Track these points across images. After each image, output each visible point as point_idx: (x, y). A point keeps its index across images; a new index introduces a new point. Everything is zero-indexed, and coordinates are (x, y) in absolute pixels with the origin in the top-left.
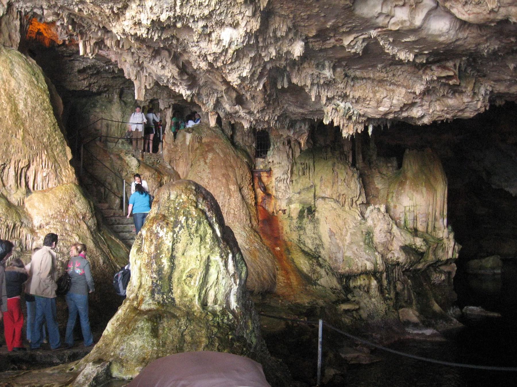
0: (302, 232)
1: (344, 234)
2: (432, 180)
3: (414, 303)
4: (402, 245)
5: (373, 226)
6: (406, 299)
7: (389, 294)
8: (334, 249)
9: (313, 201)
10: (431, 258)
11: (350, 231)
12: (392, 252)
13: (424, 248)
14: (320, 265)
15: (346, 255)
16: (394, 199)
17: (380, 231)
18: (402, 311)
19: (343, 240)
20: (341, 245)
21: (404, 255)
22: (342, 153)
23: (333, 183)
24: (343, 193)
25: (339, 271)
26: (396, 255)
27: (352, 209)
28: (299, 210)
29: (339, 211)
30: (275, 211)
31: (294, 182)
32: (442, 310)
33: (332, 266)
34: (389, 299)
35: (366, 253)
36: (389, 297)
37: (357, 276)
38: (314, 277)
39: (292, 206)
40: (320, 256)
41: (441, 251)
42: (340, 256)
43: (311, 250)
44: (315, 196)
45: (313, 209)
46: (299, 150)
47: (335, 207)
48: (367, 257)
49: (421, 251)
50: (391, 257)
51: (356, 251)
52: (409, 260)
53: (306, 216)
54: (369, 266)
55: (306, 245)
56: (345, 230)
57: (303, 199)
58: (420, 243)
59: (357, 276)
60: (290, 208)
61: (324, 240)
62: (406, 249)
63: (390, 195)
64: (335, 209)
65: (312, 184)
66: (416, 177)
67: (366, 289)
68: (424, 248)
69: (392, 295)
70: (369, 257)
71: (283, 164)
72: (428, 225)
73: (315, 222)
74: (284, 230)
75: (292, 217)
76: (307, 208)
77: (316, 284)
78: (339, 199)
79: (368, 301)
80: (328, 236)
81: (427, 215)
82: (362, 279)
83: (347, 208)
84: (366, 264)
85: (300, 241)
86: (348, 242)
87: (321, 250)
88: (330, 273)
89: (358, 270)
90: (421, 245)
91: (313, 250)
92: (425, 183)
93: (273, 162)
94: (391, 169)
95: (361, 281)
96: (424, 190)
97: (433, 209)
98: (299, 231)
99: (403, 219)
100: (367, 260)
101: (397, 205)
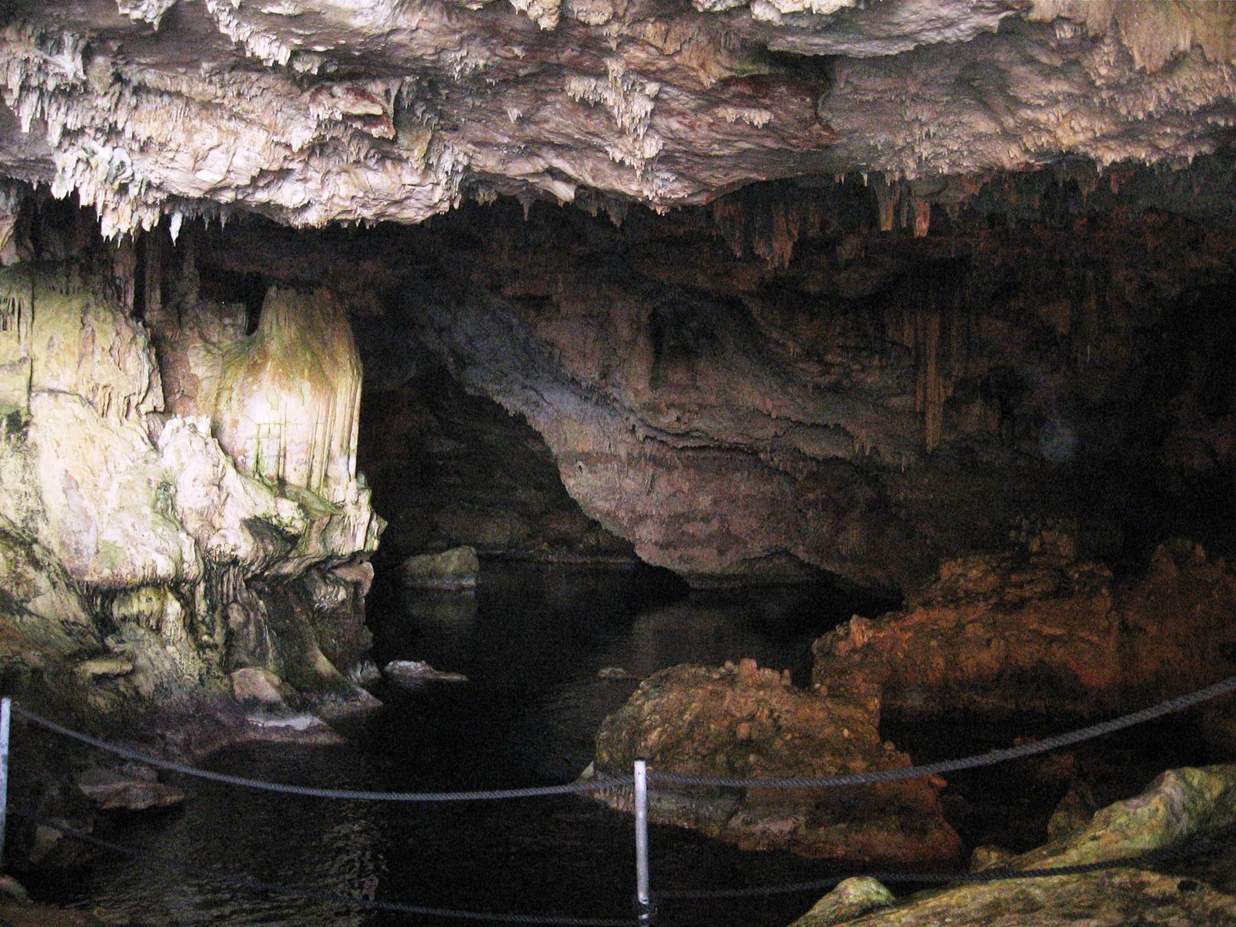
1: (101, 485)
4: (248, 517)
5: (176, 468)
7: (211, 635)
10: (314, 549)
11: (118, 479)
14: (36, 564)
16: (234, 403)
17: (195, 480)
18: (241, 676)
20: (92, 512)
22: (110, 281)
23: (82, 356)
24: (104, 382)
25: (87, 578)
32: (335, 671)
36: (211, 641)
37: (132, 590)
38: (18, 593)
40: (35, 541)
41: (339, 532)
42: (88, 540)
43: (12, 524)
44: (30, 387)
45: (24, 419)
47: (81, 417)
49: (293, 531)
50: (219, 546)
51: (131, 529)
52: (261, 554)
54: (165, 568)
56: (104, 475)
59: (132, 590)
62: (258, 527)
63: (225, 395)
64: (82, 422)
66: (289, 353)
67: (153, 622)
69: (219, 638)
70: (165, 545)
72: (311, 471)
77: (22, 611)
78: (94, 397)
81: (312, 447)
84: (154, 562)
86: (111, 505)
87: (41, 525)
88: (62, 584)
89: (135, 576)
90: (293, 518)
91: (19, 524)
94: (231, 331)
95: (141, 604)
96: (307, 386)
97: (325, 434)
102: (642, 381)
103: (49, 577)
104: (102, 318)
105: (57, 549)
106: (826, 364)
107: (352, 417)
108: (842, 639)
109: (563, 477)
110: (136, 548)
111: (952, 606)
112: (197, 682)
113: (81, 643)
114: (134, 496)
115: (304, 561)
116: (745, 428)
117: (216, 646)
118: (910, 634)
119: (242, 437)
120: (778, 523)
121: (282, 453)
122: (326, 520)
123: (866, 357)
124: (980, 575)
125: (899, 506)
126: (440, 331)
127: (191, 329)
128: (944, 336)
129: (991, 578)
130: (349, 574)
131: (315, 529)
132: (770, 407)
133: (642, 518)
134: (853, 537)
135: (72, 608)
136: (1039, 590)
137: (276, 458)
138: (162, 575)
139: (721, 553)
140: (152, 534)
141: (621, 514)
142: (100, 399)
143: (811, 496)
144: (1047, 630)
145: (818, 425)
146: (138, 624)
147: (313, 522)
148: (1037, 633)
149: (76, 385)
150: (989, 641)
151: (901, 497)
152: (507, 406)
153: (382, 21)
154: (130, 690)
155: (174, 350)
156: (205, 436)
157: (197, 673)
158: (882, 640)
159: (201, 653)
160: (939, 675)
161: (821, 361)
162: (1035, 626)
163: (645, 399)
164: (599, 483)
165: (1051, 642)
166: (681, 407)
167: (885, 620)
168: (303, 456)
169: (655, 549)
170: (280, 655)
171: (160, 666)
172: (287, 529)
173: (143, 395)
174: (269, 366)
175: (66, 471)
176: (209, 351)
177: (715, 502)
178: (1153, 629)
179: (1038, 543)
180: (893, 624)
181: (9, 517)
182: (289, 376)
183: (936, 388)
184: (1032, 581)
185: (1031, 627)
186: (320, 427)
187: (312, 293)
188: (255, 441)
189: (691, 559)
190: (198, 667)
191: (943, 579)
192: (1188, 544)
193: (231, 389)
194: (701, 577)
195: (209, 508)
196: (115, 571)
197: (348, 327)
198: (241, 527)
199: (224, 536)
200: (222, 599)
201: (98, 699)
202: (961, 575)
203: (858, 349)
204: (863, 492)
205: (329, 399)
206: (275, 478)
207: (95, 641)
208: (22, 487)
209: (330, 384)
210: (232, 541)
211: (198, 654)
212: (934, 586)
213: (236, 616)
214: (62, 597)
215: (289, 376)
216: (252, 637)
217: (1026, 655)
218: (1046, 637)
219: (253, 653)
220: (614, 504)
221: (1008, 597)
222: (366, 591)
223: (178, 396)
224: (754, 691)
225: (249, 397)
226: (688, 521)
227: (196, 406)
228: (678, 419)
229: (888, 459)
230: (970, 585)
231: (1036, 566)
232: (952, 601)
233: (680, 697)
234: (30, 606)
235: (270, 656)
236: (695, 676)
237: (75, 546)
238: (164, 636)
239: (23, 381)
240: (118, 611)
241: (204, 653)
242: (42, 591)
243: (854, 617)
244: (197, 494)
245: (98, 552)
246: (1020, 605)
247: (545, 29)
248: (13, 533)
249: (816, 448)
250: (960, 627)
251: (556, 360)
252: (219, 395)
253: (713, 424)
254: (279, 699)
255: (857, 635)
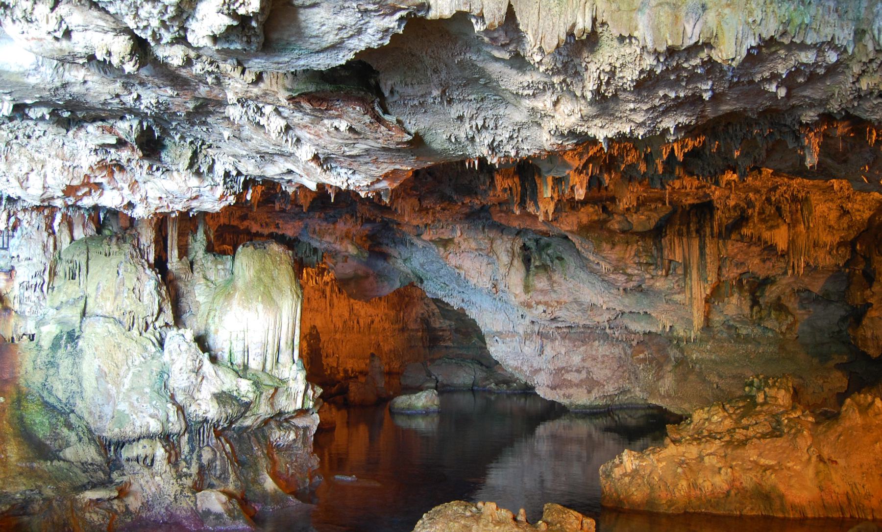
0: (52, 371)
1: (122, 374)
2: (274, 293)
3: (231, 480)
4: (216, 391)
5: (170, 362)
6: (218, 473)
7: (189, 468)
8: (99, 399)
9: (79, 321)
10: (264, 410)
11: (133, 370)
12: (198, 402)
13: (251, 396)
14: (70, 426)
15: (119, 408)
16: (216, 319)
17: (181, 369)
18: (201, 496)
19: (118, 385)
20: (113, 391)
21: (217, 406)
22: (137, 247)
23: (117, 294)
24: (129, 309)
25: (104, 434)
26: (204, 407)
27: (144, 334)
28: (55, 335)
29: (121, 339)
30: (15, 336)
31: (55, 289)
32: (276, 487)
33: (93, 427)
34: (186, 475)
35: (152, 405)
36: (189, 472)
37: (134, 441)
38: (54, 446)
39: (45, 329)
40: (73, 411)
41: (284, 398)
42: (108, 410)
43: (60, 401)
44: (84, 314)
45: (77, 334)
46: (68, 240)
47: (113, 332)
48: (152, 411)
49: (246, 400)
50: (195, 411)
51: (136, 403)
52: (224, 415)
53: (63, 346)
54: (155, 427)
55: (54, 392)
56: (125, 367)
57: (63, 317)
58: (247, 388)
59: (134, 441)
60: (41, 333)
61: (86, 384)
62: (222, 398)
63: (212, 314)
64: (113, 335)
65: (82, 294)
66: (250, 287)
67: (148, 461)
68: (251, 396)
69: (194, 469)
70: (156, 412)
71: (35, 260)
72: (265, 360)
73: (77, 355)
74: (23, 368)
75: (41, 347)
76: (68, 333)
78: (124, 319)
79: (147, 482)
80: (94, 377)
81: (265, 345)
82: (140, 447)
83: (135, 332)
84: (148, 423)
85: (45, 385)
86: (126, 387)
87: (78, 402)
88: (85, 439)
89: (134, 432)
90: (248, 391)
91: (64, 401)
92: (262, 297)
93: (18, 256)
94: (222, 273)
95: (137, 450)
96: (260, 307)
97: (274, 336)
98: (48, 369)
99: (227, 351)
100: (151, 416)
101: (220, 329)
102: (518, 288)
103: (77, 435)
104: (129, 270)
105: (86, 416)
106: (629, 275)
107: (294, 325)
108: (617, 466)
109: (488, 346)
110: (136, 414)
111: (695, 443)
112: (172, 500)
113: (92, 477)
114: (141, 381)
115: (258, 418)
116: (589, 315)
117: (191, 475)
118: (664, 463)
119: (220, 341)
120: (623, 373)
121: (246, 349)
122: (272, 391)
123: (654, 270)
124: (720, 420)
125: (695, 362)
126: (405, 260)
127: (198, 272)
128: (702, 254)
129: (728, 422)
130: (300, 422)
131: (263, 396)
132: (601, 302)
133: (537, 371)
134: (668, 383)
135: (90, 454)
136: (760, 431)
137: (242, 353)
138: (153, 431)
139: (589, 392)
140: (148, 405)
141: (525, 368)
142: (127, 320)
143: (641, 356)
144: (763, 461)
145: (634, 313)
146: (138, 462)
147: (261, 393)
148: (756, 463)
149: (113, 312)
150: (720, 469)
151: (694, 356)
152: (452, 304)
153: (49, 79)
154: (121, 508)
155: (186, 286)
156: (189, 341)
157: (173, 493)
158: (644, 467)
159: (179, 480)
160: (683, 493)
161: (625, 273)
162: (755, 458)
163: (522, 299)
164: (509, 350)
165: (765, 471)
166: (546, 304)
167: (648, 453)
168: (259, 351)
169: (548, 390)
170: (238, 478)
171: (148, 490)
172: (242, 399)
173: (155, 316)
174: (237, 295)
175: (99, 366)
176: (208, 286)
177: (583, 360)
178: (842, 462)
179: (763, 396)
180: (651, 456)
181: (59, 396)
182: (248, 301)
183: (699, 290)
184: (757, 423)
185: (752, 459)
186: (271, 332)
187: (265, 248)
188: (228, 342)
189: (569, 396)
190: (175, 490)
191: (695, 422)
192: (870, 398)
193: (216, 310)
194: (577, 406)
195: (189, 387)
196: (122, 430)
197: (290, 268)
198: (211, 398)
199: (199, 404)
200: (199, 444)
201: (93, 515)
202: (707, 419)
203: (648, 264)
204: (673, 353)
205: (276, 313)
206: (242, 365)
207: (103, 476)
208: (70, 377)
209: (277, 305)
210: (204, 407)
211: (177, 481)
212: (688, 427)
213: (207, 455)
214: (85, 447)
215: (248, 301)
216: (218, 468)
217: (748, 480)
218: (762, 466)
219: (219, 478)
220: (520, 362)
221: (737, 436)
222: (313, 433)
223: (188, 314)
224: (492, 526)
225: (225, 315)
226: (567, 372)
227: (197, 321)
228: (544, 312)
229: (682, 334)
230: (713, 427)
231: (760, 413)
232: (696, 439)
233: (443, 528)
234: (61, 454)
235: (231, 479)
236: (455, 512)
237: (99, 414)
238: (154, 470)
239: (79, 310)
240: (125, 453)
241: (181, 480)
242: (71, 444)
243: (626, 451)
244: (182, 378)
245: (113, 417)
246: (743, 443)
247: (129, 73)
248: (59, 407)
249: (639, 327)
250: (701, 458)
251: (463, 277)
252: (208, 314)
253: (568, 313)
254: (223, 511)
255: (627, 463)
